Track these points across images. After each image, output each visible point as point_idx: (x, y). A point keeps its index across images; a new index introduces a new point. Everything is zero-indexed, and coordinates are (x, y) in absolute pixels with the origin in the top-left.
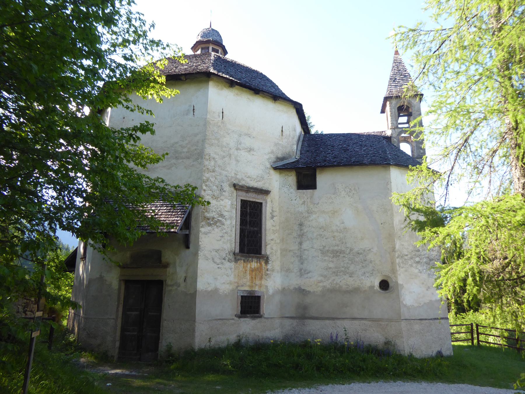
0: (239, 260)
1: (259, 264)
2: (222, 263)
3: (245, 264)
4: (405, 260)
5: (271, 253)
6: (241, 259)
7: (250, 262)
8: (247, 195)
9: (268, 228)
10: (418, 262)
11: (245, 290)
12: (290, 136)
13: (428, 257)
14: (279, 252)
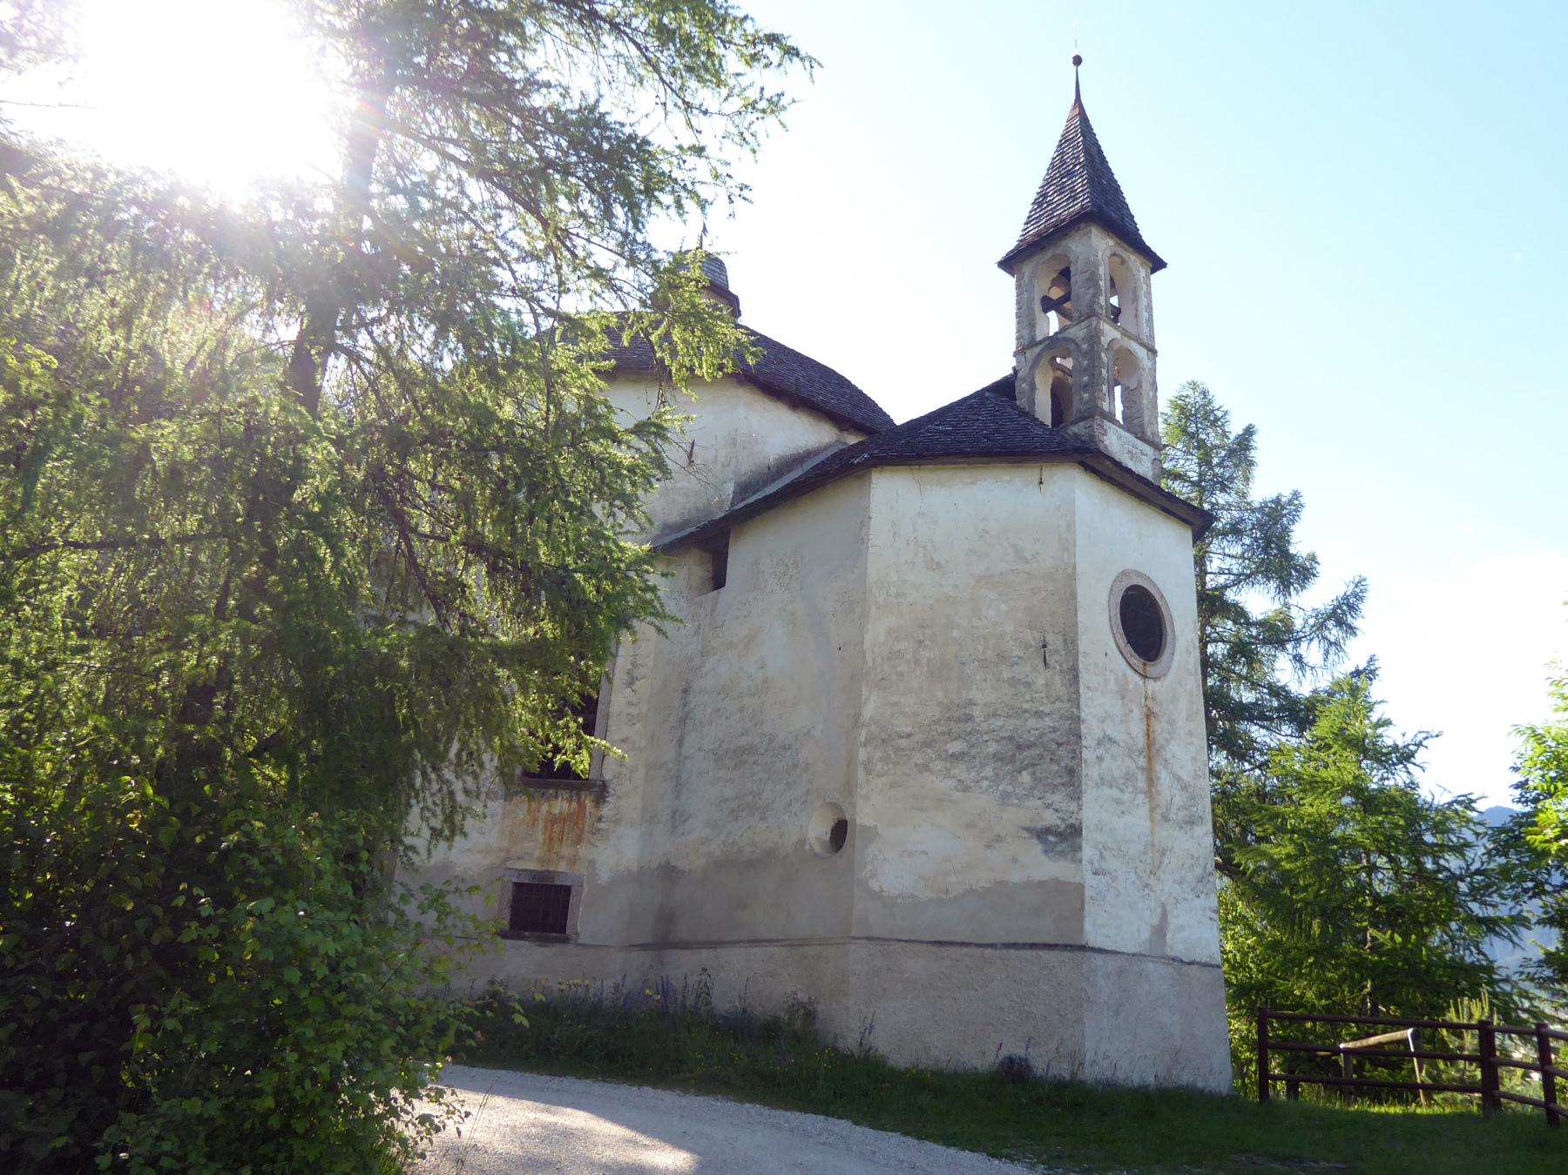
0: (516, 793)
1: (574, 804)
3: (534, 805)
4: (898, 749)
5: (618, 776)
7: (548, 800)
10: (955, 757)
12: (715, 462)
13: (1010, 738)
14: (642, 771)
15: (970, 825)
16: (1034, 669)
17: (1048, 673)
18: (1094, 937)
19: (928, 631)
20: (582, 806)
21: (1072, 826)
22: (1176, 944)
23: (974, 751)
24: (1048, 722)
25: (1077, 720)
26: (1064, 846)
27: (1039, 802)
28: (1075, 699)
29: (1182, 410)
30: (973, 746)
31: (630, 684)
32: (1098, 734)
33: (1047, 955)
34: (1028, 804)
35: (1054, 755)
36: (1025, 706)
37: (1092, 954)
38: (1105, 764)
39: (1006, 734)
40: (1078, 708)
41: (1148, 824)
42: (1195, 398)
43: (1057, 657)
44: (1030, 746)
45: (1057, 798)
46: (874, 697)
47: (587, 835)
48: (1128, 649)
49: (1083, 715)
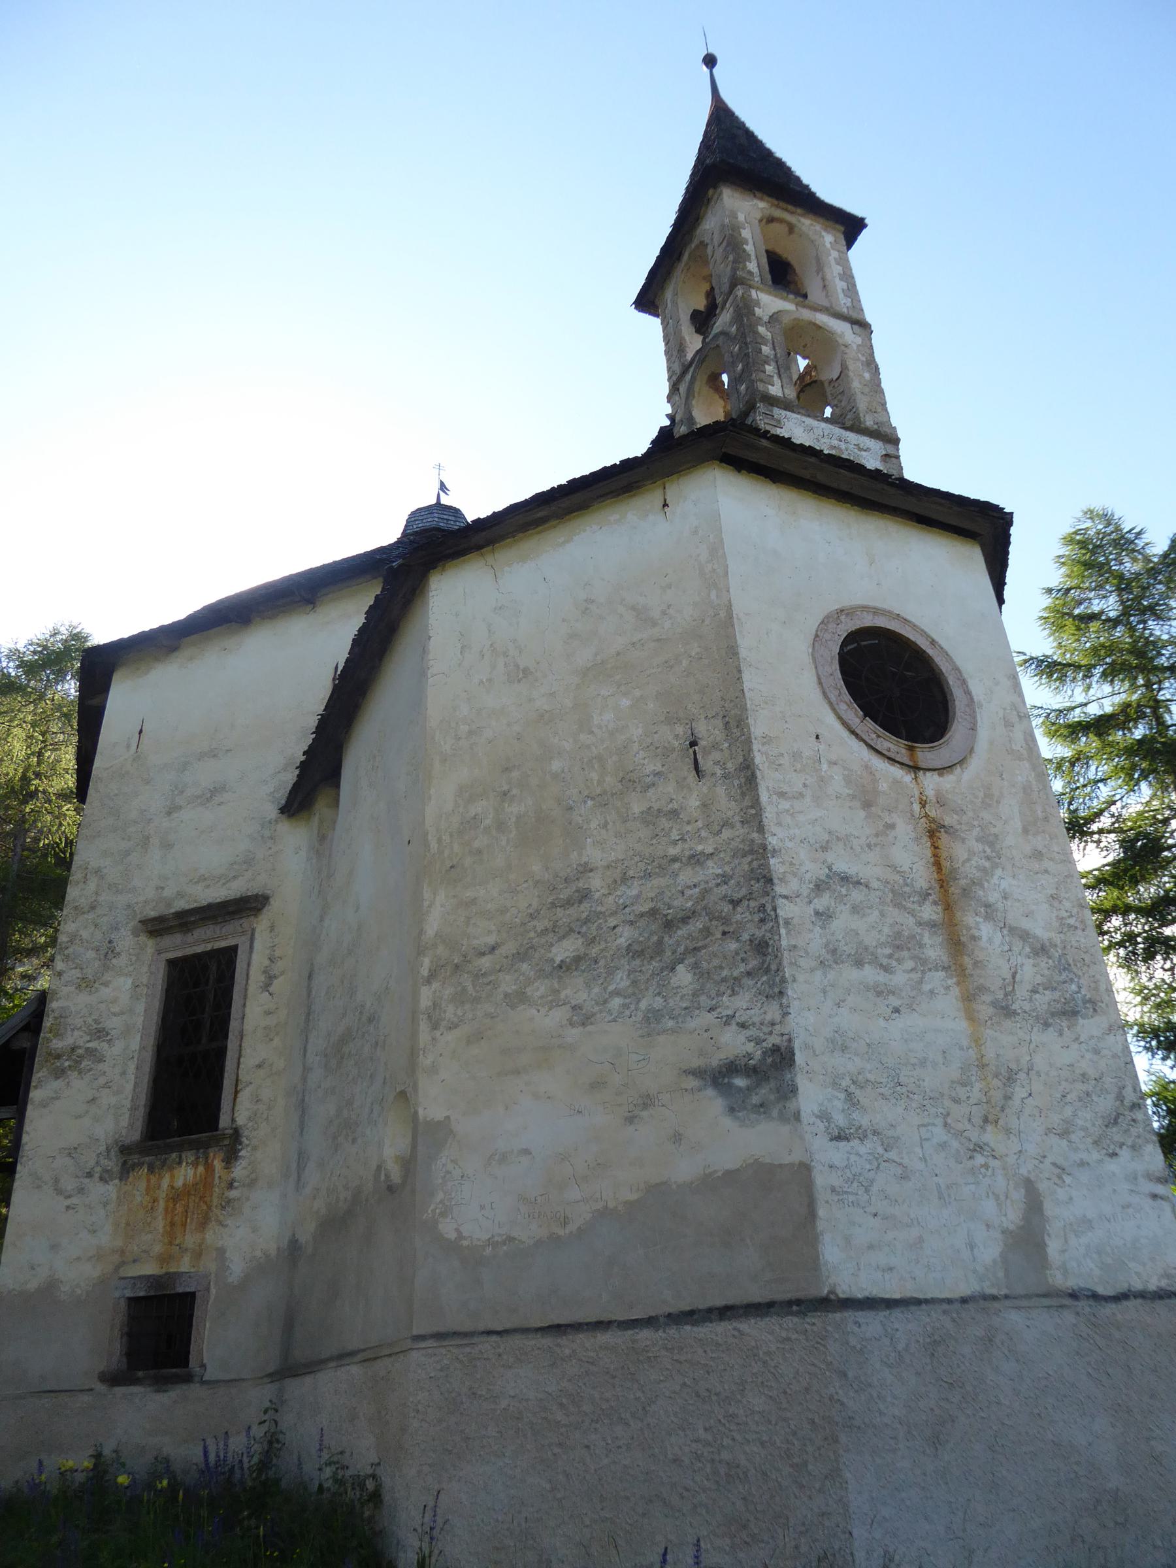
1: (201, 1169)
2: (81, 1190)
3: (153, 1179)
4: (478, 976)
6: (141, 1165)
8: (190, 938)
9: (249, 1025)
11: (140, 1277)
13: (653, 912)
15: (597, 1085)
16: (681, 784)
17: (704, 787)
18: (847, 1267)
19: (515, 774)
20: (209, 1168)
21: (776, 1049)
22: (1073, 1259)
23: (594, 951)
24: (713, 869)
25: (760, 852)
26: (765, 1092)
27: (710, 1017)
28: (754, 817)
29: (1083, 544)
30: (592, 941)
31: (266, 987)
32: (813, 870)
33: (752, 1328)
34: (692, 1024)
35: (728, 926)
36: (673, 851)
37: (849, 1315)
38: (837, 925)
39: (645, 908)
40: (761, 829)
41: (963, 1025)
42: (1093, 528)
43: (716, 755)
44: (685, 920)
45: (741, 1003)
46: (441, 897)
47: (217, 1211)
48: (869, 728)
49: (773, 841)
